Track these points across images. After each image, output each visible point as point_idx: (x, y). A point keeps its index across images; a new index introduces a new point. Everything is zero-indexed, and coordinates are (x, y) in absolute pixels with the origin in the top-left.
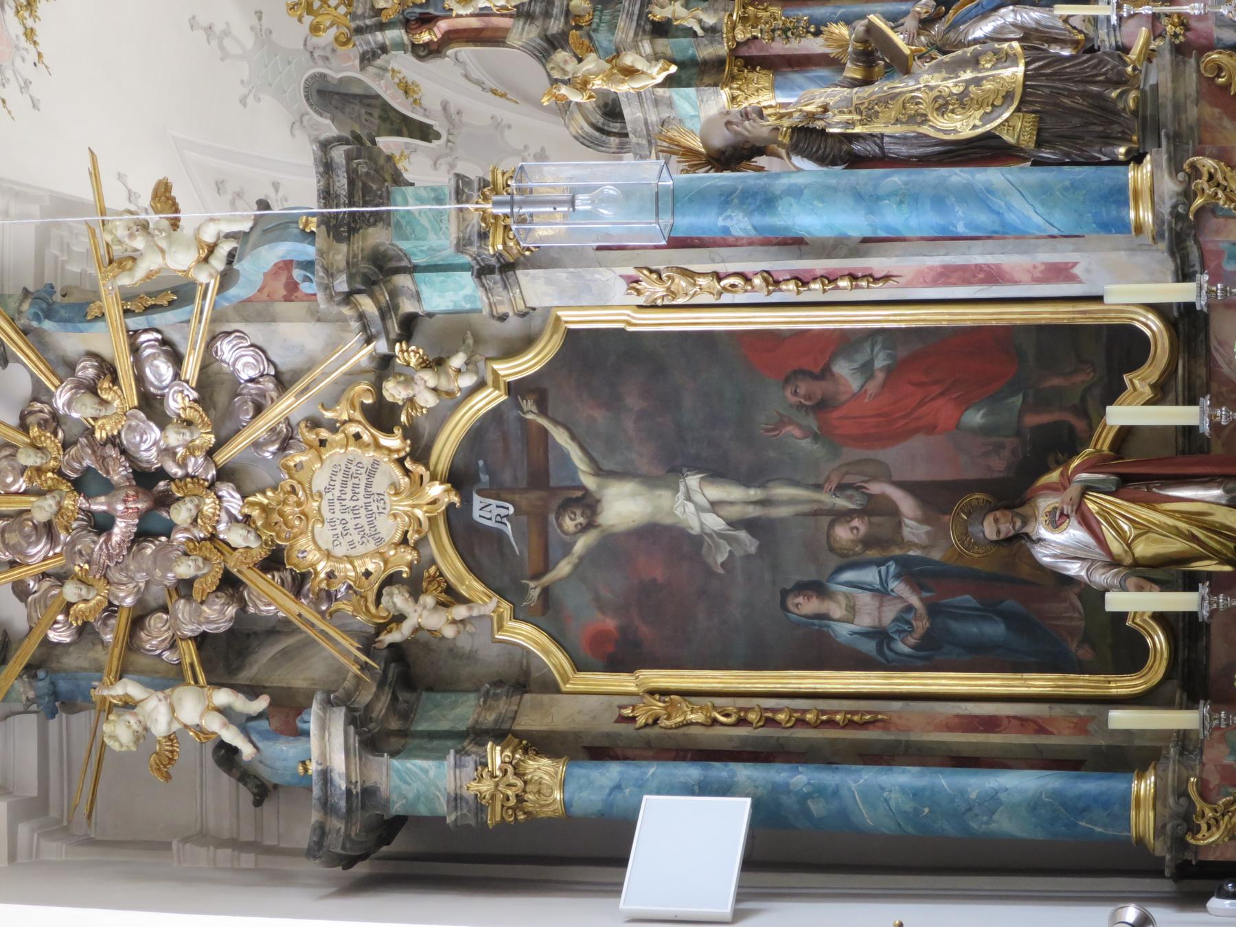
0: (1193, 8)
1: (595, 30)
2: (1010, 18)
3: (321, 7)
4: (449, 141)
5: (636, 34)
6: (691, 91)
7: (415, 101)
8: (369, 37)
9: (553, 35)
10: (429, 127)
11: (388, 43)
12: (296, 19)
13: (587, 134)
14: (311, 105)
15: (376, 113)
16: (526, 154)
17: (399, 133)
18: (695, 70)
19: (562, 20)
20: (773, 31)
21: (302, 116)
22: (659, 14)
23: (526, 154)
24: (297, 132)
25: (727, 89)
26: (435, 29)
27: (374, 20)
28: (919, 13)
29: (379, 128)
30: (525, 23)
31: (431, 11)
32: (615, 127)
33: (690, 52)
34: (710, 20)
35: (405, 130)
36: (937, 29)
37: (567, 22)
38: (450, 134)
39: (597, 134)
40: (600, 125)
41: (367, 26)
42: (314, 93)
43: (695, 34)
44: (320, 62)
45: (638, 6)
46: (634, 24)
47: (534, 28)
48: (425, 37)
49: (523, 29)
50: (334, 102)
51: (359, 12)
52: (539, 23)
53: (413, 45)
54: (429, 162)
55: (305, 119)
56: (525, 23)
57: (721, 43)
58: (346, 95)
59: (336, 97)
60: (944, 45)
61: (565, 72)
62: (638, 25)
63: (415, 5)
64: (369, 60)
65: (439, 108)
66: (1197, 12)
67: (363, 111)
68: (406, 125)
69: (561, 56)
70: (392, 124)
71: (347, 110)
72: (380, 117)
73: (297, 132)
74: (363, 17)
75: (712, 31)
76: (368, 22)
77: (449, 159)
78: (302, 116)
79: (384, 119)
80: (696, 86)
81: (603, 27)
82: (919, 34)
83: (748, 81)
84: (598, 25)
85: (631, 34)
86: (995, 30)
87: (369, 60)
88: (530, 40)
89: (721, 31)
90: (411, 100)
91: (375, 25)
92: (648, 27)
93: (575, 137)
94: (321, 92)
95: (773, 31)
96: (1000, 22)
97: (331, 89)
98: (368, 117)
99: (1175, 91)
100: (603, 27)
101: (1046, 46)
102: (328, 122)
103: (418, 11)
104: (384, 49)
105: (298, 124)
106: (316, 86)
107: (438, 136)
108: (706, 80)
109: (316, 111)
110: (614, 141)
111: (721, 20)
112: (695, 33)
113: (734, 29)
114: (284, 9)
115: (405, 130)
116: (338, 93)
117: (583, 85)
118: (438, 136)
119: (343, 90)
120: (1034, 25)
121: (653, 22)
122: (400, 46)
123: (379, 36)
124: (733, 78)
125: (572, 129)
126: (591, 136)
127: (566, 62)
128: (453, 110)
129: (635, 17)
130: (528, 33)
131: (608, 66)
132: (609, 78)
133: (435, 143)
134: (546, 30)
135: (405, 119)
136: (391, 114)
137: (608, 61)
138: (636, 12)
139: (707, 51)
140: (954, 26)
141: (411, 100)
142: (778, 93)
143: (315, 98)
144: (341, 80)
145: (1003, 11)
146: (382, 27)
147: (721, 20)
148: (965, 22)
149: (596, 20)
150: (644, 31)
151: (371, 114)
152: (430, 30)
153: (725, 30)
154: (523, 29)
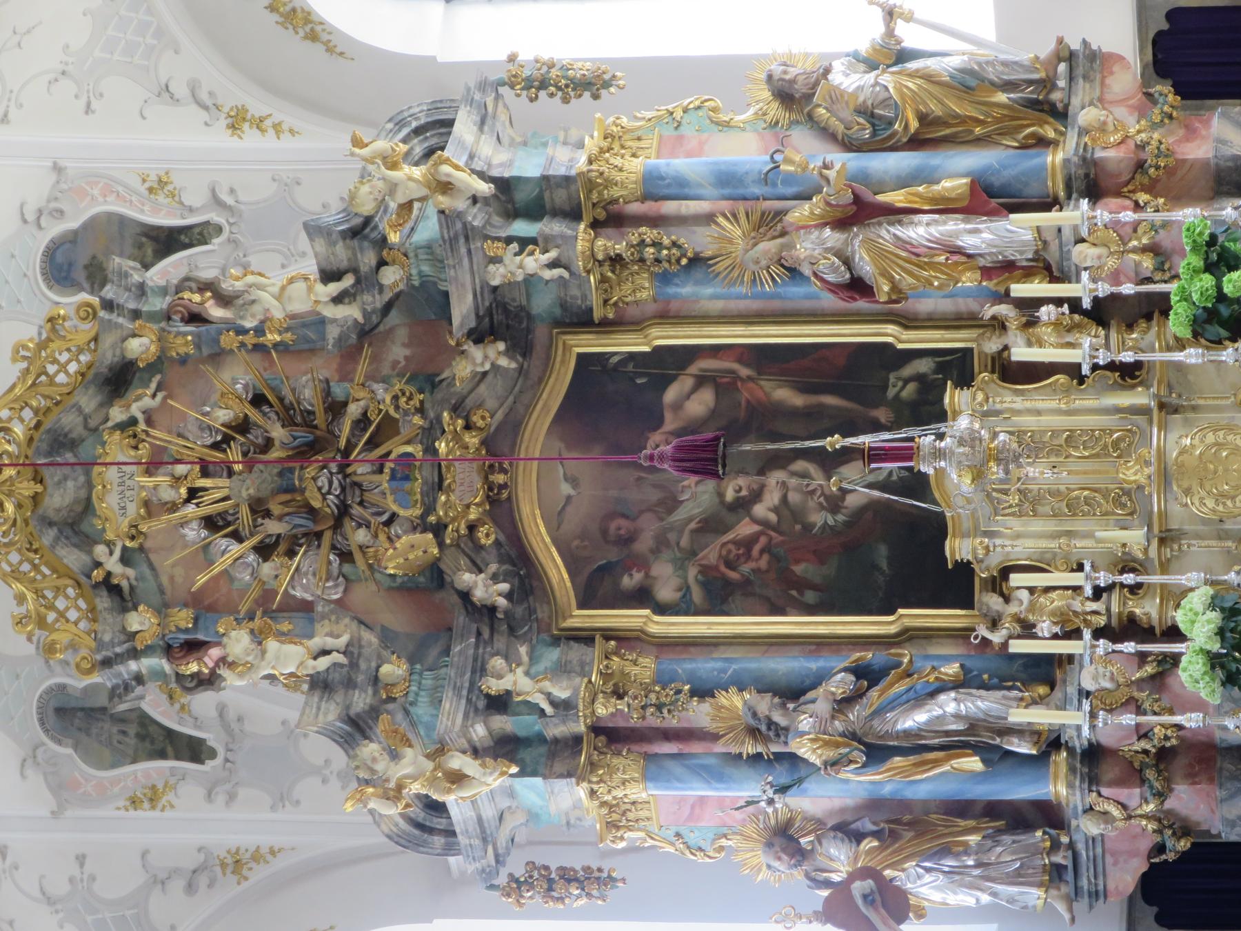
0: (1190, 720)
1: (411, 704)
2: (951, 708)
3: (57, 620)
4: (227, 760)
5: (466, 716)
6: (538, 781)
7: (183, 707)
8: (121, 668)
9: (358, 715)
10: (200, 742)
11: (144, 671)
12: (24, 636)
13: (404, 832)
14: (46, 731)
15: (132, 730)
16: (327, 772)
17: (162, 755)
18: (543, 749)
19: (370, 691)
20: (644, 708)
21: (35, 748)
22: (494, 686)
23: (327, 772)
24: (29, 772)
25: (585, 785)
26: (206, 659)
27: (126, 646)
28: (833, 694)
29: (136, 751)
30: (321, 699)
31: (201, 637)
32: (439, 823)
33: (537, 728)
34: (562, 694)
35: (169, 749)
36: (856, 714)
37: (376, 693)
38: (229, 750)
39: (416, 832)
40: (420, 820)
41: (117, 655)
42: (51, 713)
43: (542, 712)
44: (58, 669)
45: (468, 675)
46: (464, 701)
47: (332, 706)
48: (194, 667)
49: (319, 708)
50: (77, 721)
51: (107, 638)
52: (339, 697)
53: (177, 674)
54: (201, 792)
55: (40, 752)
56: (321, 699)
57: (577, 721)
58: (92, 709)
59: (80, 714)
60: (866, 734)
61: (373, 771)
62: (469, 701)
63: (179, 630)
64: (120, 696)
65: (214, 713)
66: (1193, 725)
67: (115, 730)
68: (171, 743)
69: (370, 749)
70: (152, 742)
71: (94, 731)
72: (138, 735)
73: (29, 772)
74: (113, 644)
75: (564, 707)
76: (118, 650)
77: (228, 786)
78: (35, 748)
79: (141, 737)
80: (545, 777)
81: (424, 699)
82: (833, 717)
83: (612, 771)
84: (417, 694)
85: (459, 720)
86: (929, 722)
87: (120, 696)
88: (329, 724)
89: (576, 707)
90: (177, 706)
91: (128, 651)
92: (481, 704)
93: (389, 837)
94: (60, 711)
95: (644, 708)
96: (939, 712)
97: (73, 704)
98: (121, 737)
99: (1160, 618)
100: (424, 699)
101: (998, 740)
102: (70, 751)
103: (183, 637)
104: (139, 679)
105: (30, 761)
106: (53, 704)
107: (213, 754)
108: (559, 767)
109: (53, 738)
110: (438, 841)
111: (576, 692)
112: (543, 711)
113: (593, 702)
114: (10, 622)
115: (169, 749)
116: (82, 709)
117: (394, 794)
118: (213, 754)
119: (88, 705)
120: (981, 716)
121: (488, 696)
122: (159, 675)
123: (133, 666)
124: (593, 766)
125: (384, 827)
126: (409, 835)
127: (374, 760)
128: (232, 715)
129: (465, 692)
130: (326, 714)
131: (430, 765)
132: (432, 781)
133: (210, 765)
134: (348, 707)
135: (170, 734)
136: (152, 729)
137: (428, 756)
138: (467, 685)
139: (557, 729)
140: (879, 712)
141: (177, 706)
142: (650, 785)
143: (51, 718)
144: (85, 689)
145: (942, 697)
146: (135, 654)
147: (576, 692)
148: (892, 709)
149: (414, 688)
150: (476, 710)
151: (124, 733)
152: (200, 660)
153: (581, 707)
154: (319, 708)
